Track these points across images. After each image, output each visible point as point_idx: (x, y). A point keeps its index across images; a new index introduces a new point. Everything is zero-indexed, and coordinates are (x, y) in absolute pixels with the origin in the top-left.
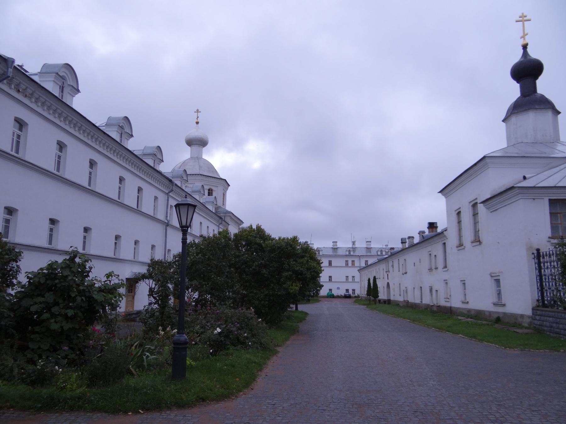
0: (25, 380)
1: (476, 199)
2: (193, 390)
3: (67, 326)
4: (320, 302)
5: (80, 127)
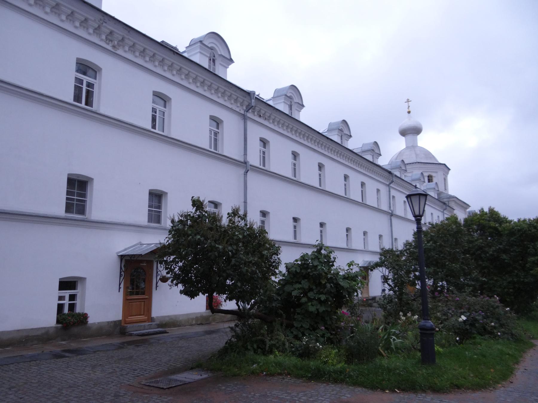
0: (294, 353)
2: (446, 376)
3: (322, 309)
5: (291, 129)
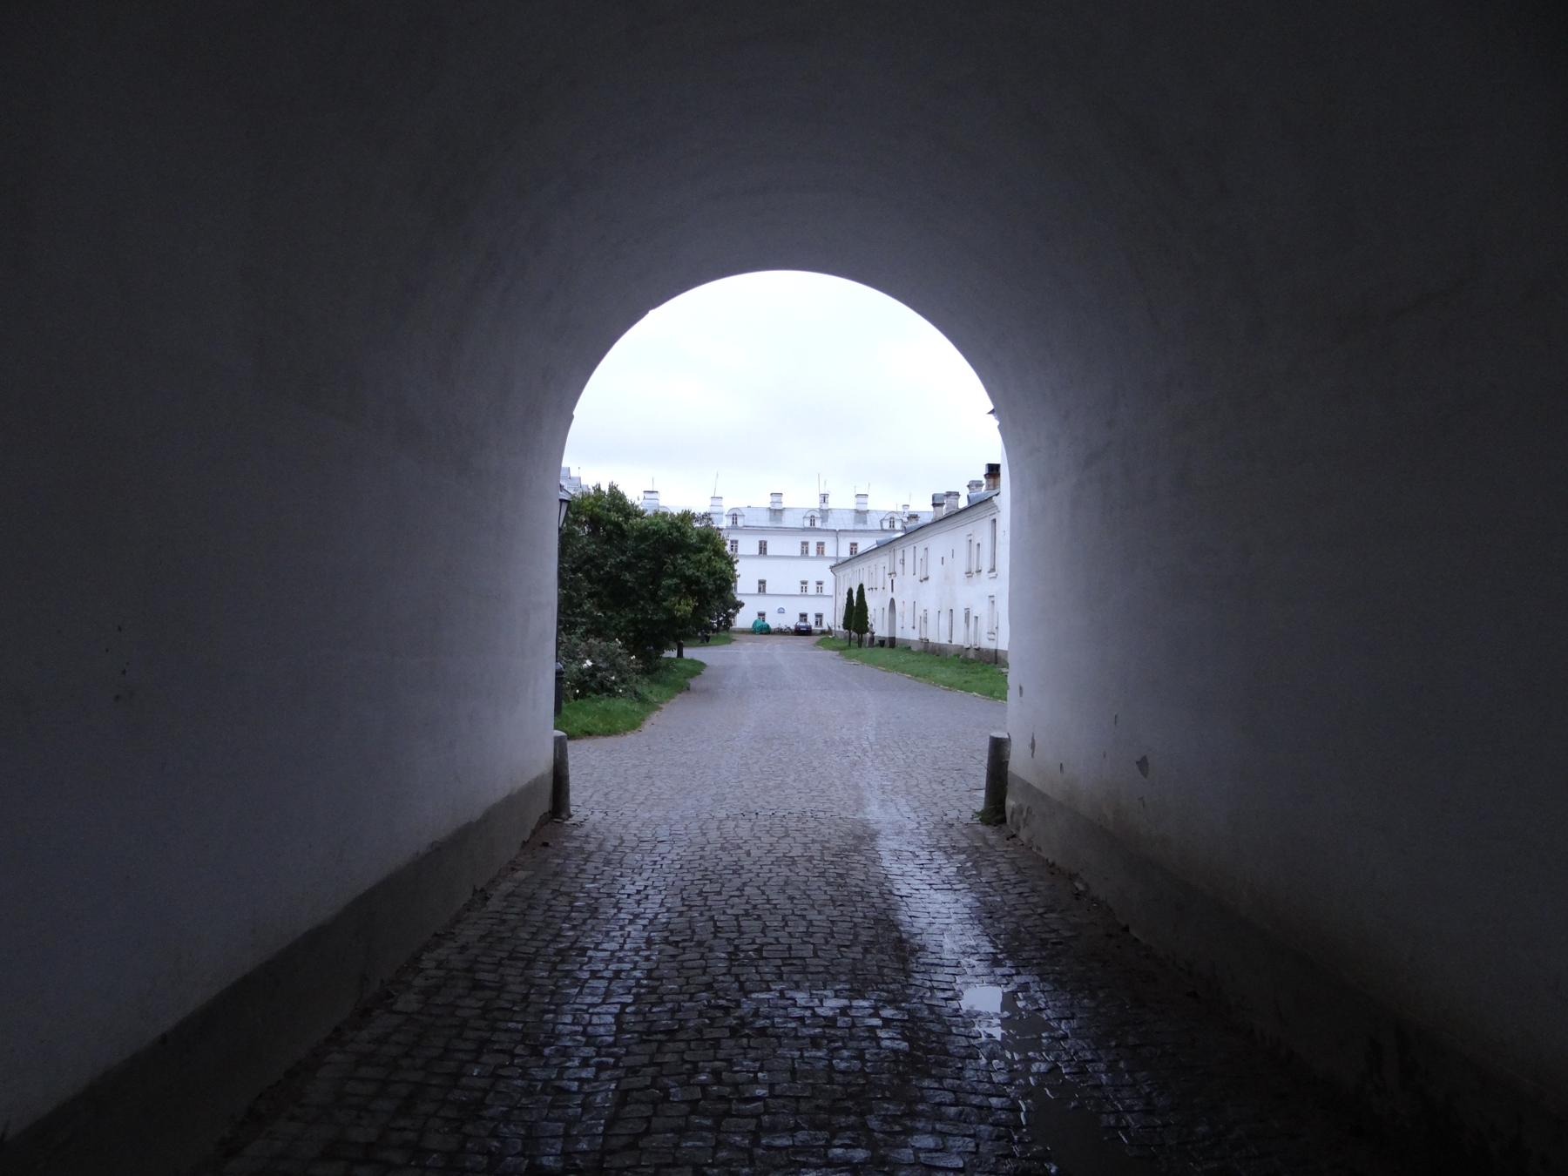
4: (734, 644)
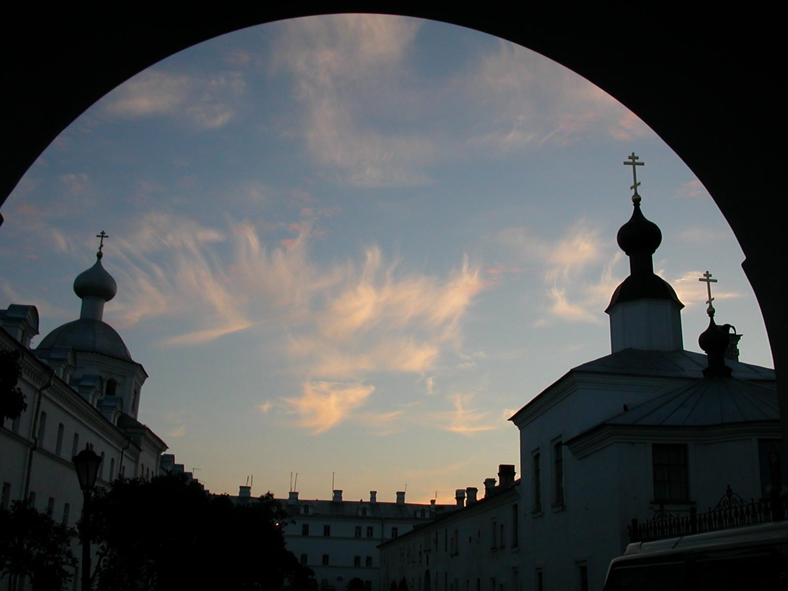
1: (561, 436)
